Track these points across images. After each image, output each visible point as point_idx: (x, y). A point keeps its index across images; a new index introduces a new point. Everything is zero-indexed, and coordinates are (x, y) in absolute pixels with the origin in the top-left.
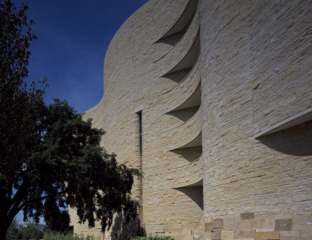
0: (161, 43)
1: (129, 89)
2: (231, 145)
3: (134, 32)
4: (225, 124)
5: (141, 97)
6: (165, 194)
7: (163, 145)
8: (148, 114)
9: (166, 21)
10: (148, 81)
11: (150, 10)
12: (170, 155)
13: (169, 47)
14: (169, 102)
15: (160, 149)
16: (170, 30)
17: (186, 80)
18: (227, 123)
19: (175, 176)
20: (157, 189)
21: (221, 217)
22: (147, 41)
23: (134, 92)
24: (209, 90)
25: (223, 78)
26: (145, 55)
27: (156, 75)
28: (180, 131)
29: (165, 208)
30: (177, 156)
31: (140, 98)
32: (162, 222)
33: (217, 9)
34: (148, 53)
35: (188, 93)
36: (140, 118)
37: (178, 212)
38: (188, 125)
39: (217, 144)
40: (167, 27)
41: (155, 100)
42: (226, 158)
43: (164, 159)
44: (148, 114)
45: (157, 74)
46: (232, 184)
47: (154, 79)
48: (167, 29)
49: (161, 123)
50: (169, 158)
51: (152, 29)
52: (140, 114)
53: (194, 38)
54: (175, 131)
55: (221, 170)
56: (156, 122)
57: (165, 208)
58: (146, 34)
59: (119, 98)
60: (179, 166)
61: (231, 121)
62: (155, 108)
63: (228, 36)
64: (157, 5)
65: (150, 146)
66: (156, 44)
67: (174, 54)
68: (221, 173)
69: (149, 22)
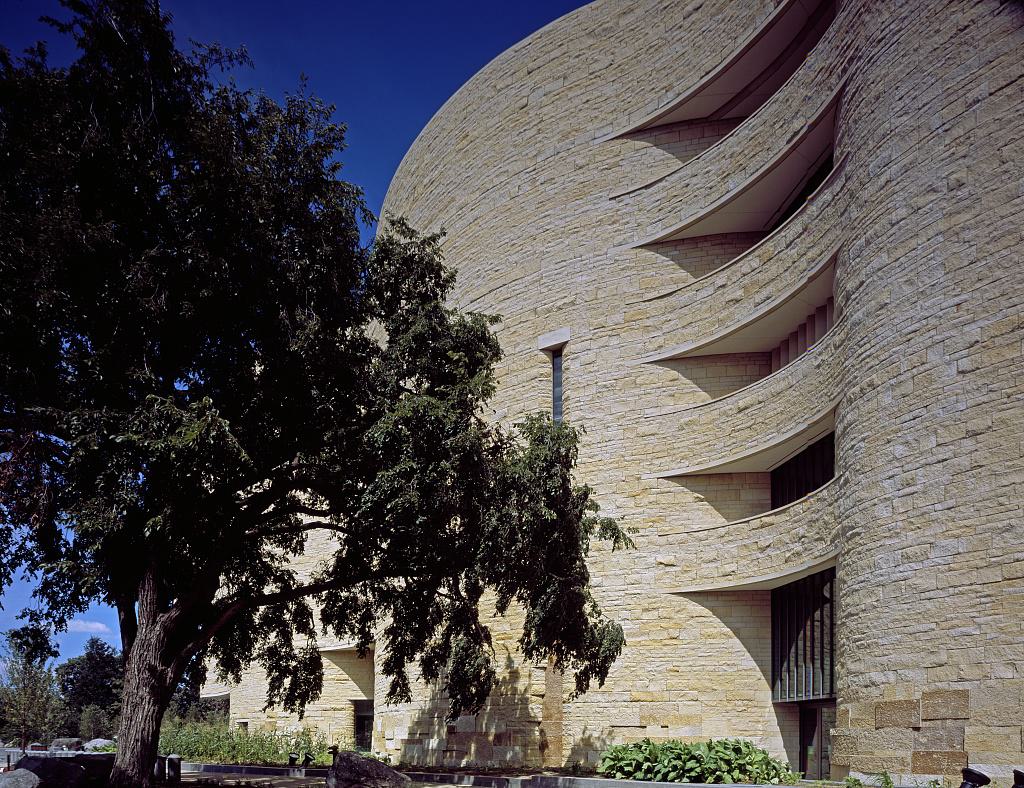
0: (640, 140)
1: (517, 272)
2: (1010, 463)
3: (540, 92)
4: (985, 399)
5: (565, 300)
6: (647, 610)
7: (643, 457)
8: (591, 356)
9: (664, 72)
10: (591, 255)
11: (604, 30)
12: (666, 490)
13: (668, 159)
14: (666, 327)
15: (633, 470)
16: (681, 104)
17: (739, 265)
18: (993, 396)
19: (682, 555)
20: (622, 593)
21: (959, 687)
22: (590, 126)
23: (537, 284)
24: (907, 290)
25: (980, 255)
26: (582, 171)
27: (620, 239)
28: (704, 419)
29: (649, 651)
30: (688, 496)
31: (559, 303)
32: (636, 695)
33: (961, 30)
34: (591, 166)
35: (748, 305)
36: (557, 368)
37: (690, 666)
38: (741, 404)
39: (946, 460)
40: (671, 95)
41: (618, 318)
42: (987, 503)
43: (646, 501)
44: (591, 356)
45: (625, 236)
46: (1010, 586)
47: (612, 252)
48: (670, 100)
49: (636, 391)
50: (662, 499)
51: (609, 91)
52: (556, 353)
53: (796, 133)
54: (687, 419)
55: (963, 539)
56: (620, 383)
57: (649, 651)
58: (586, 106)
59: (472, 296)
60: (696, 528)
61: (1015, 389)
62: (614, 341)
63: (1011, 121)
64: (630, 18)
65: (597, 459)
66: (618, 141)
67: (694, 180)
68: (961, 550)
69: (596, 66)
